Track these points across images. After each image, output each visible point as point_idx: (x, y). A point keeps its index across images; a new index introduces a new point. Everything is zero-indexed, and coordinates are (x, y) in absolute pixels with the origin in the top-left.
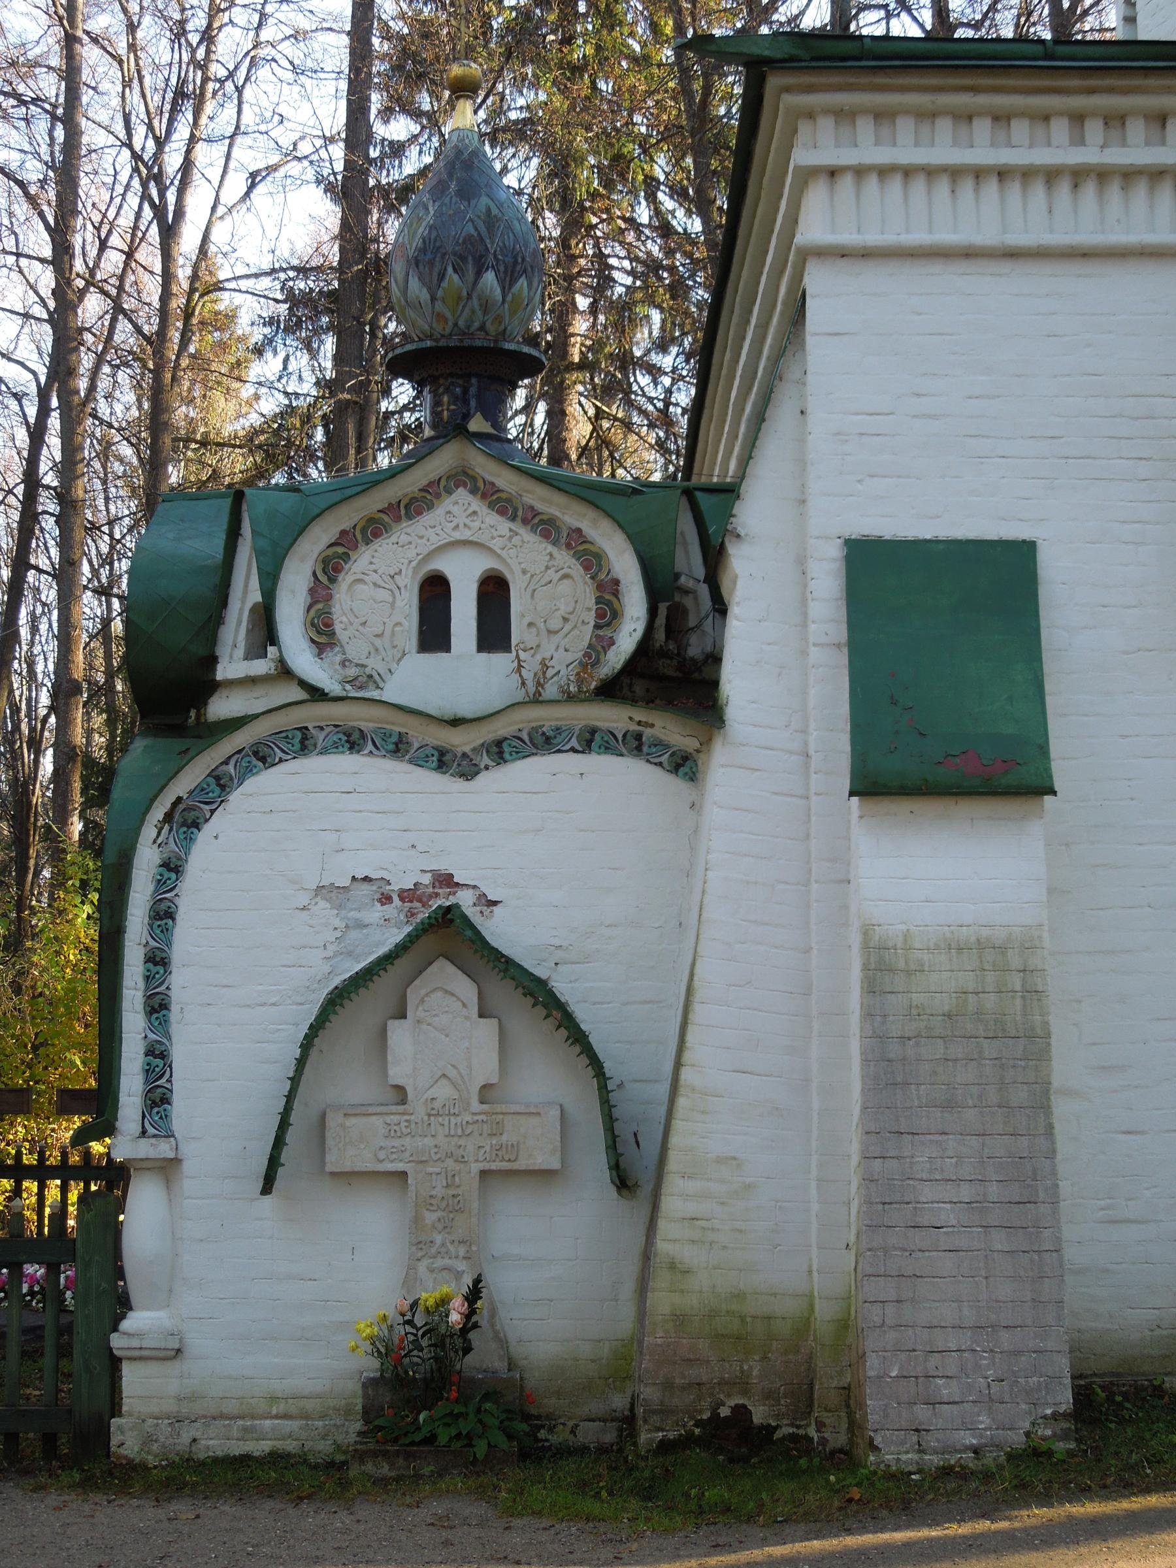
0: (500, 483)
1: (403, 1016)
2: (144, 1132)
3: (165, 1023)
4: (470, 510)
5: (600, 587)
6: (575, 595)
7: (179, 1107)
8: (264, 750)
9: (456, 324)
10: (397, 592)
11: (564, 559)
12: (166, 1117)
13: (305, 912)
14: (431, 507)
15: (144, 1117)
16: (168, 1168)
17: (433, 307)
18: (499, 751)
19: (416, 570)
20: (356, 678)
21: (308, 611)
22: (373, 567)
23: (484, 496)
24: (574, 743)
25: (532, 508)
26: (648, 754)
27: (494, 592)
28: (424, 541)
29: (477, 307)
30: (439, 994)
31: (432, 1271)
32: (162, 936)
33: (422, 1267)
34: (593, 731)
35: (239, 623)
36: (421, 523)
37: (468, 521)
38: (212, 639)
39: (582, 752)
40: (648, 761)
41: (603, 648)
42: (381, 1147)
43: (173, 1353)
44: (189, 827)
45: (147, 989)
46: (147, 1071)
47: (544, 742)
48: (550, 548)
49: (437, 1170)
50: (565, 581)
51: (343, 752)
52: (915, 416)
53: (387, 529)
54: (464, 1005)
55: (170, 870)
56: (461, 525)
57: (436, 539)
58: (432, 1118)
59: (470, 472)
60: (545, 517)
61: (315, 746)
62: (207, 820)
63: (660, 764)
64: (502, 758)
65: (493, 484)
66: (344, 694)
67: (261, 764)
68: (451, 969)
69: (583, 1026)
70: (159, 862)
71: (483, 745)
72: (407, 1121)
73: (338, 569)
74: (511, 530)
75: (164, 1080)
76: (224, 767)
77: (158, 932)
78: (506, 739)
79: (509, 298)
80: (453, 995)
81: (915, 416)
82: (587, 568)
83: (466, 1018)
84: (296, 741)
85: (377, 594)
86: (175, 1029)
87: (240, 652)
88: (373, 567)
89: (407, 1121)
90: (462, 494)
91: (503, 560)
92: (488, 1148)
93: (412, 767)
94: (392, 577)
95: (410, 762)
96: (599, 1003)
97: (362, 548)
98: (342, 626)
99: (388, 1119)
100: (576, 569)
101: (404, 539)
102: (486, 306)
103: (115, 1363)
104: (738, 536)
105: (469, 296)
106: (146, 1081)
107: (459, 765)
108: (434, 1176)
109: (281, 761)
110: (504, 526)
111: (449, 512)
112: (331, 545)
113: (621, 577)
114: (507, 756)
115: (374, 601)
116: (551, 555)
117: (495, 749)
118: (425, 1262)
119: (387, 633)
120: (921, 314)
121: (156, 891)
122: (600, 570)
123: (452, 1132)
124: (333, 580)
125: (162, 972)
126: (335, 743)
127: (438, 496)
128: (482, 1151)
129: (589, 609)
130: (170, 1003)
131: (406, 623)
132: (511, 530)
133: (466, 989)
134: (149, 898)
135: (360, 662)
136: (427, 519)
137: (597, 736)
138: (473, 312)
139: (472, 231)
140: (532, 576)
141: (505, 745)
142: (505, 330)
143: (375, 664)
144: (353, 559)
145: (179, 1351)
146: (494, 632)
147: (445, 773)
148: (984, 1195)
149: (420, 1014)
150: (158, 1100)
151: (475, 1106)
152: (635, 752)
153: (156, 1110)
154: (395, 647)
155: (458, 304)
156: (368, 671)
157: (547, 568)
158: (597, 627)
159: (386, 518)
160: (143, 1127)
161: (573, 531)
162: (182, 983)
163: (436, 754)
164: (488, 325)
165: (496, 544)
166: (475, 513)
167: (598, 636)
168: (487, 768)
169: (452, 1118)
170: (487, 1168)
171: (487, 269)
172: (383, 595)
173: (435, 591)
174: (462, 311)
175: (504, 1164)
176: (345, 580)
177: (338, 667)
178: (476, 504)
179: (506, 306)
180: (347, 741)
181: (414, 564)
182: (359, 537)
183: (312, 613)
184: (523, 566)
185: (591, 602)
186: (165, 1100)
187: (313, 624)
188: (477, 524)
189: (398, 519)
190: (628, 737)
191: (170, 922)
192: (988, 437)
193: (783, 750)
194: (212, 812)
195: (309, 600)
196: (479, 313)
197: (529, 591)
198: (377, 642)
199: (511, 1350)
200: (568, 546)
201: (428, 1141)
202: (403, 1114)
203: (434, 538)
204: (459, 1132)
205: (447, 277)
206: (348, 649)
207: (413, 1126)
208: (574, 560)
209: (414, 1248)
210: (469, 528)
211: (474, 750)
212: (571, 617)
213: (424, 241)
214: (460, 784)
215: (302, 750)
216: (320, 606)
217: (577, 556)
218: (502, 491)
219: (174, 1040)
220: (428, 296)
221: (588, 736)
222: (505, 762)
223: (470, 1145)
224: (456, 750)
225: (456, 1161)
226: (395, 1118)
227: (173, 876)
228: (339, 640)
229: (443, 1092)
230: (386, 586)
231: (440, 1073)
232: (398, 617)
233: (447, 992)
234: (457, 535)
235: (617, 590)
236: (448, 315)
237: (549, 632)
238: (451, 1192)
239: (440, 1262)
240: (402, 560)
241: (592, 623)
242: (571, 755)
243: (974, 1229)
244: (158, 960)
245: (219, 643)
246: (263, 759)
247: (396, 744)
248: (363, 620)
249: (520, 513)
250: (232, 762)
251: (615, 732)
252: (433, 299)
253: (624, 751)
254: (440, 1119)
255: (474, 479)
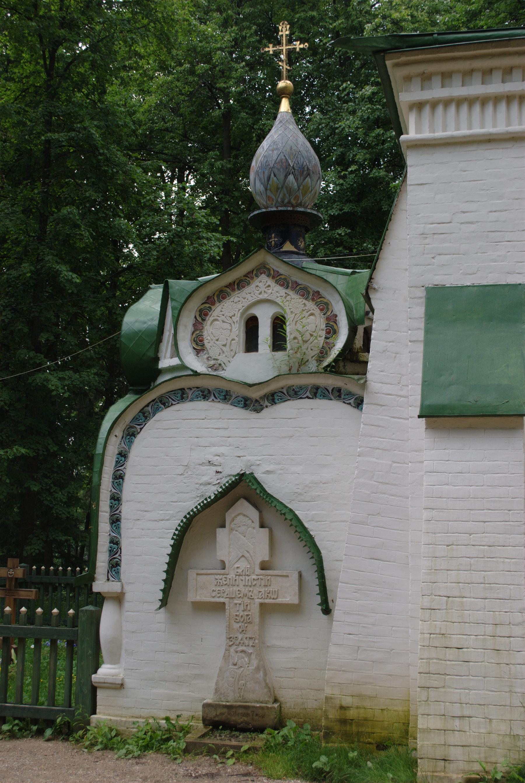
0: (281, 271)
1: (223, 526)
2: (108, 580)
3: (118, 528)
4: (267, 285)
5: (328, 319)
6: (317, 322)
7: (124, 567)
8: (165, 400)
9: (277, 201)
10: (233, 324)
11: (311, 305)
12: (118, 573)
13: (182, 476)
14: (249, 284)
15: (108, 572)
16: (119, 599)
17: (266, 194)
18: (273, 398)
19: (242, 314)
20: (214, 365)
21: (192, 335)
22: (222, 313)
23: (273, 278)
24: (308, 394)
25: (296, 282)
26: (344, 399)
27: (278, 324)
28: (246, 300)
29: (286, 193)
30: (241, 517)
31: (237, 652)
32: (118, 487)
33: (232, 649)
34: (317, 388)
35: (168, 341)
36: (244, 292)
37: (266, 290)
38: (157, 350)
39: (312, 398)
40: (344, 402)
41: (329, 348)
42: (213, 590)
43: (119, 686)
44: (131, 436)
45: (111, 512)
46: (110, 551)
47: (294, 393)
48: (304, 301)
49: (239, 602)
50: (311, 317)
51: (200, 400)
52: (461, 223)
53: (229, 295)
54: (253, 522)
55: (122, 456)
56: (263, 292)
57: (252, 299)
58: (237, 577)
59: (267, 266)
60: (302, 286)
61: (188, 397)
62: (138, 433)
63: (349, 404)
64: (274, 402)
65: (278, 272)
66: (208, 373)
67: (163, 406)
68: (246, 504)
69: (311, 533)
70: (117, 452)
71: (265, 396)
72: (226, 578)
73: (206, 315)
74: (286, 293)
75: (117, 555)
76: (146, 408)
77: (116, 485)
78: (276, 393)
79: (301, 187)
80: (247, 517)
81: (461, 223)
82: (322, 310)
83: (254, 528)
84: (179, 395)
85: (224, 324)
86: (123, 531)
87: (168, 354)
88: (222, 313)
89: (226, 578)
90: (263, 277)
91: (282, 308)
92: (263, 592)
93: (232, 407)
94: (231, 318)
95: (231, 404)
96: (319, 521)
97: (217, 304)
98: (208, 341)
99: (217, 577)
100: (317, 311)
101: (237, 299)
102: (290, 191)
103: (94, 690)
104: (374, 289)
105: (282, 187)
106: (110, 555)
107: (254, 405)
108: (238, 605)
109: (172, 405)
110: (282, 291)
111: (257, 286)
112: (203, 304)
113: (338, 313)
114: (276, 401)
115: (222, 329)
116: (304, 304)
117: (271, 398)
118: (234, 647)
119: (228, 344)
120: (465, 171)
121: (116, 466)
122: (328, 311)
123: (247, 584)
124: (204, 320)
125: (117, 504)
126: (197, 396)
127: (252, 278)
128: (261, 593)
129: (323, 330)
130: (121, 519)
131: (237, 339)
132: (286, 293)
133: (254, 514)
134: (113, 469)
135: (215, 358)
136: (247, 290)
137: (319, 391)
138: (284, 195)
139: (283, 157)
140: (296, 314)
141: (275, 396)
142: (301, 202)
143: (222, 359)
144: (213, 310)
145: (122, 685)
146: (278, 342)
147: (247, 409)
148: (485, 632)
149: (233, 526)
150: (114, 566)
151: (258, 571)
152: (338, 398)
153: (114, 569)
154: (232, 350)
155: (277, 192)
156: (219, 362)
157: (303, 310)
158: (326, 338)
159: (229, 290)
160: (108, 577)
161: (316, 292)
162: (126, 510)
163: (243, 400)
164: (292, 200)
165: (278, 301)
166: (269, 286)
167: (327, 343)
168: (267, 407)
169: (247, 577)
170: (263, 602)
171: (290, 174)
172: (227, 326)
173: (252, 325)
174: (279, 195)
175: (271, 600)
176: (209, 319)
177: (206, 360)
178: (270, 282)
179: (300, 191)
180: (202, 395)
181: (241, 311)
182: (216, 299)
183: (194, 335)
184: (291, 310)
185: (323, 326)
186: (118, 564)
187: (194, 341)
188: (270, 291)
189: (233, 290)
190: (334, 391)
191: (121, 480)
192: (501, 231)
193: (396, 395)
194: (141, 429)
195: (193, 330)
196: (287, 195)
197: (294, 322)
198: (224, 349)
199: (276, 692)
200: (313, 300)
201: (236, 588)
202: (223, 574)
203: (250, 299)
204: (250, 584)
205: (271, 179)
206: (210, 351)
207: (228, 580)
208: (315, 306)
209: (228, 640)
210: (267, 293)
211: (261, 398)
212: (314, 334)
213: (261, 164)
214: (254, 415)
215: (182, 399)
216: (198, 332)
217: (318, 304)
218: (282, 275)
219: (122, 536)
220: (264, 189)
221: (315, 391)
222: (276, 404)
223: (256, 590)
224: (253, 400)
225: (248, 598)
226: (221, 577)
227: (123, 459)
228: (206, 348)
229: (243, 565)
230: (228, 321)
231: (241, 555)
232: (233, 336)
233: (244, 515)
234: (261, 297)
235: (336, 320)
236: (274, 197)
237: (304, 341)
238: (246, 613)
239: (241, 648)
240: (236, 309)
241: (324, 336)
242: (307, 400)
243: (479, 650)
244: (116, 499)
245: (160, 351)
246: (164, 404)
247: (225, 396)
248: (217, 338)
249: (290, 285)
250: (150, 406)
251: (328, 388)
252: (266, 189)
253: (332, 398)
254: (241, 577)
255: (269, 270)
